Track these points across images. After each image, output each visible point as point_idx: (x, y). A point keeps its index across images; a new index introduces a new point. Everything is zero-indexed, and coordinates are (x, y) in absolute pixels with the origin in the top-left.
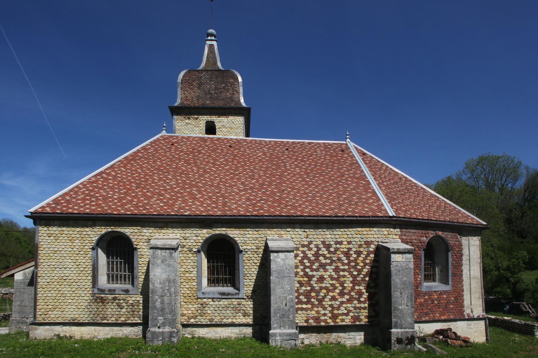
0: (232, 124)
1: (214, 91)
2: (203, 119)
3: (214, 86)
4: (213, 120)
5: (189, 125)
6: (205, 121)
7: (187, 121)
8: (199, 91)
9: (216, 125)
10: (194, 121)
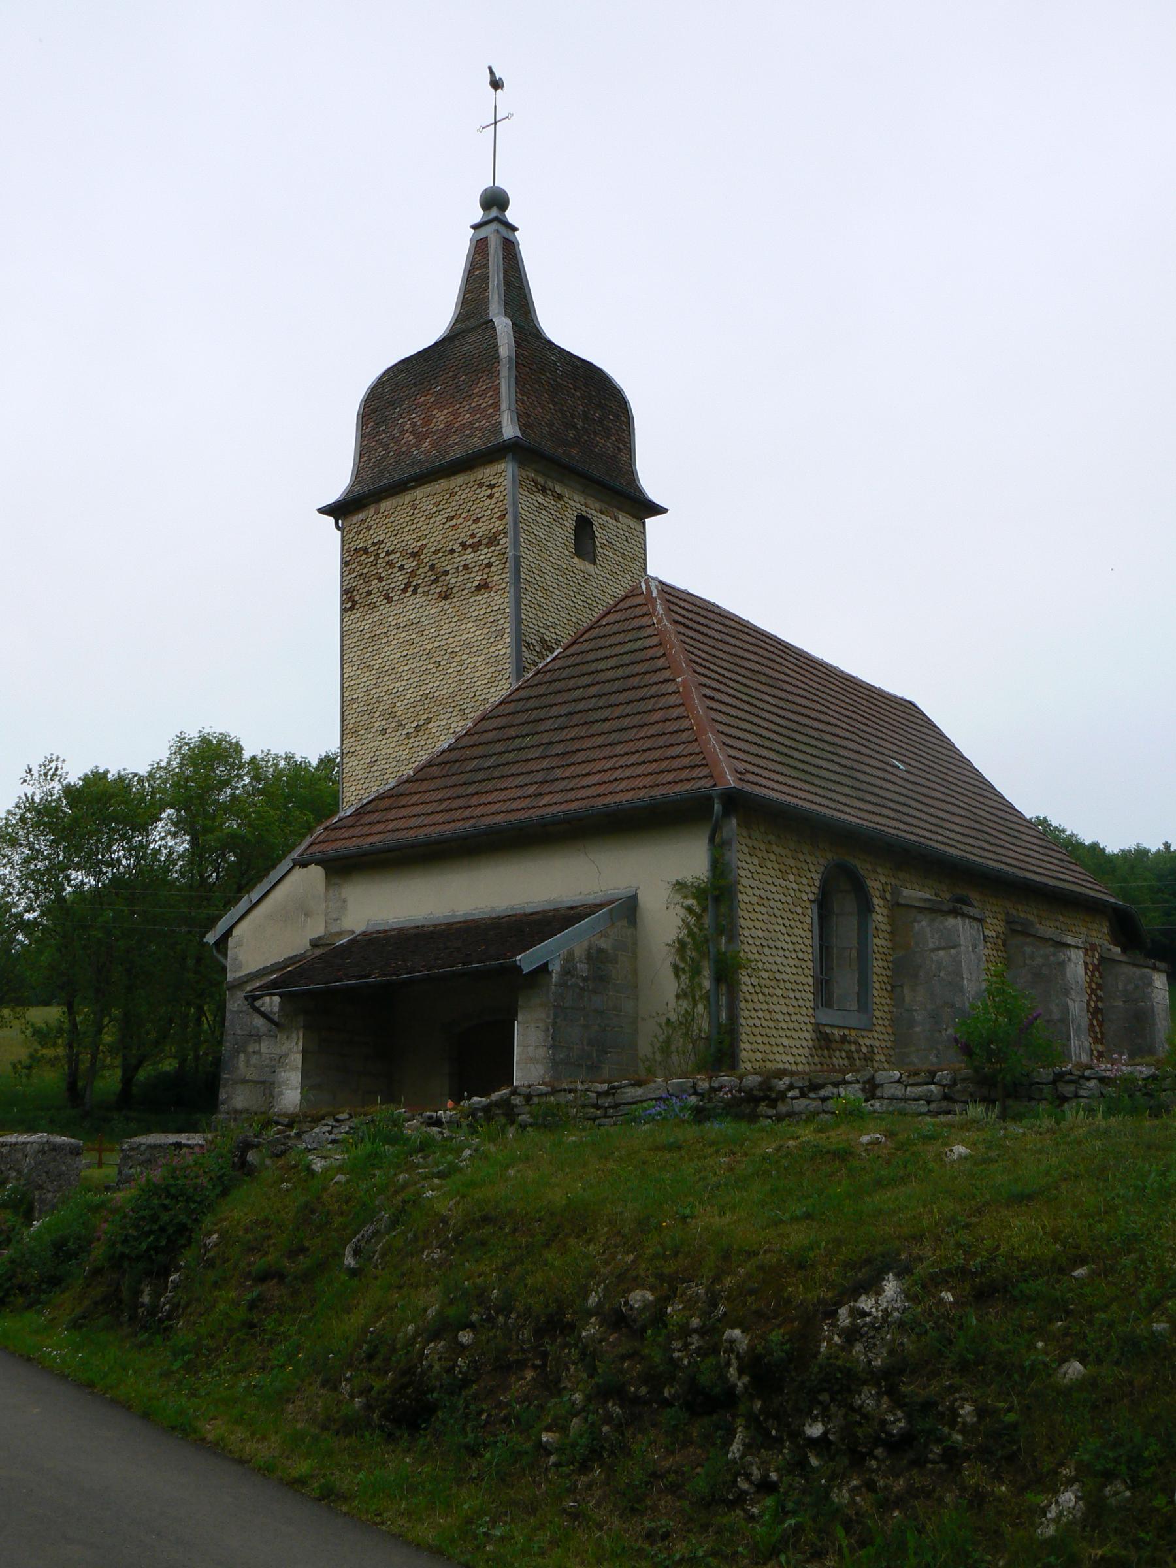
0: (625, 543)
1: (581, 423)
2: (577, 502)
3: (581, 407)
4: (590, 517)
5: (544, 512)
6: (575, 514)
7: (540, 498)
8: (551, 406)
9: (597, 534)
10: (553, 502)
